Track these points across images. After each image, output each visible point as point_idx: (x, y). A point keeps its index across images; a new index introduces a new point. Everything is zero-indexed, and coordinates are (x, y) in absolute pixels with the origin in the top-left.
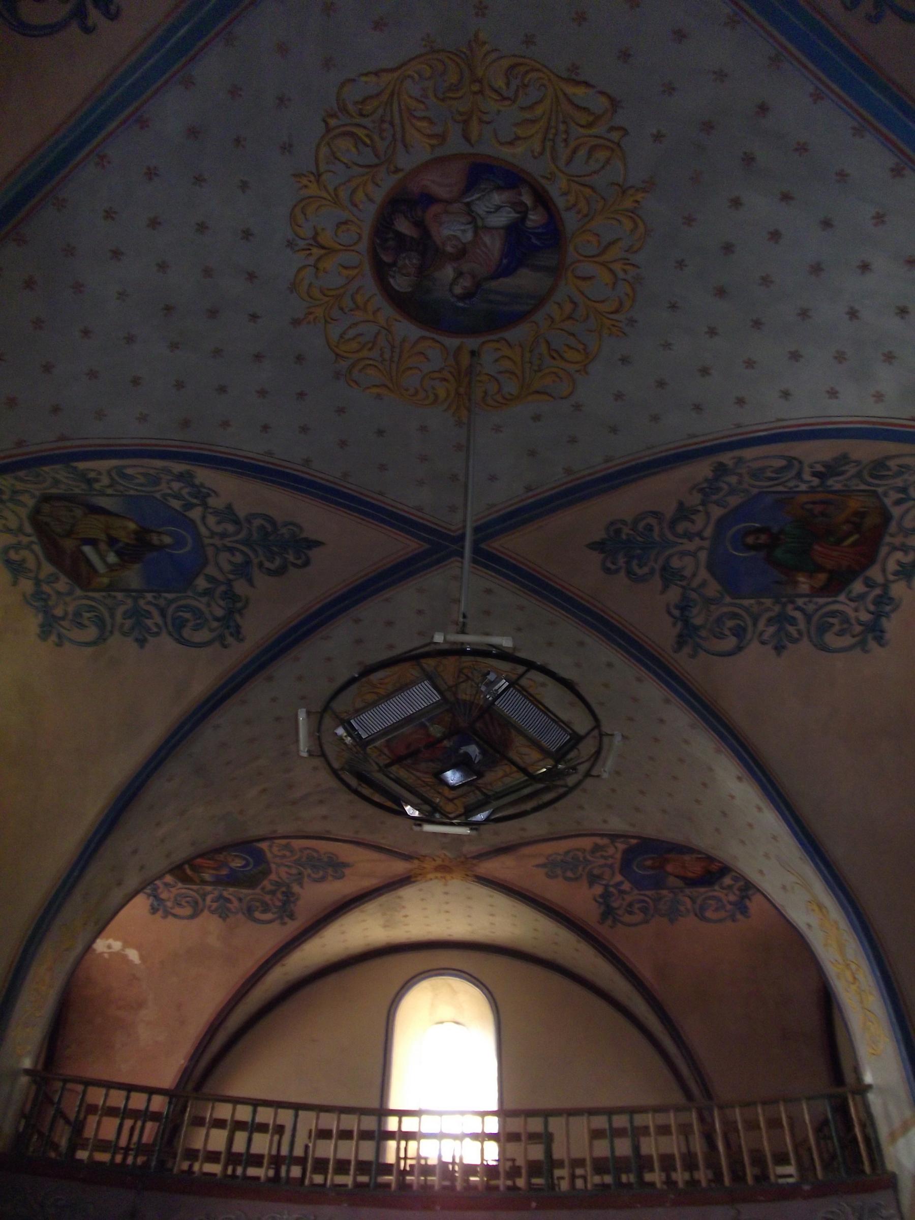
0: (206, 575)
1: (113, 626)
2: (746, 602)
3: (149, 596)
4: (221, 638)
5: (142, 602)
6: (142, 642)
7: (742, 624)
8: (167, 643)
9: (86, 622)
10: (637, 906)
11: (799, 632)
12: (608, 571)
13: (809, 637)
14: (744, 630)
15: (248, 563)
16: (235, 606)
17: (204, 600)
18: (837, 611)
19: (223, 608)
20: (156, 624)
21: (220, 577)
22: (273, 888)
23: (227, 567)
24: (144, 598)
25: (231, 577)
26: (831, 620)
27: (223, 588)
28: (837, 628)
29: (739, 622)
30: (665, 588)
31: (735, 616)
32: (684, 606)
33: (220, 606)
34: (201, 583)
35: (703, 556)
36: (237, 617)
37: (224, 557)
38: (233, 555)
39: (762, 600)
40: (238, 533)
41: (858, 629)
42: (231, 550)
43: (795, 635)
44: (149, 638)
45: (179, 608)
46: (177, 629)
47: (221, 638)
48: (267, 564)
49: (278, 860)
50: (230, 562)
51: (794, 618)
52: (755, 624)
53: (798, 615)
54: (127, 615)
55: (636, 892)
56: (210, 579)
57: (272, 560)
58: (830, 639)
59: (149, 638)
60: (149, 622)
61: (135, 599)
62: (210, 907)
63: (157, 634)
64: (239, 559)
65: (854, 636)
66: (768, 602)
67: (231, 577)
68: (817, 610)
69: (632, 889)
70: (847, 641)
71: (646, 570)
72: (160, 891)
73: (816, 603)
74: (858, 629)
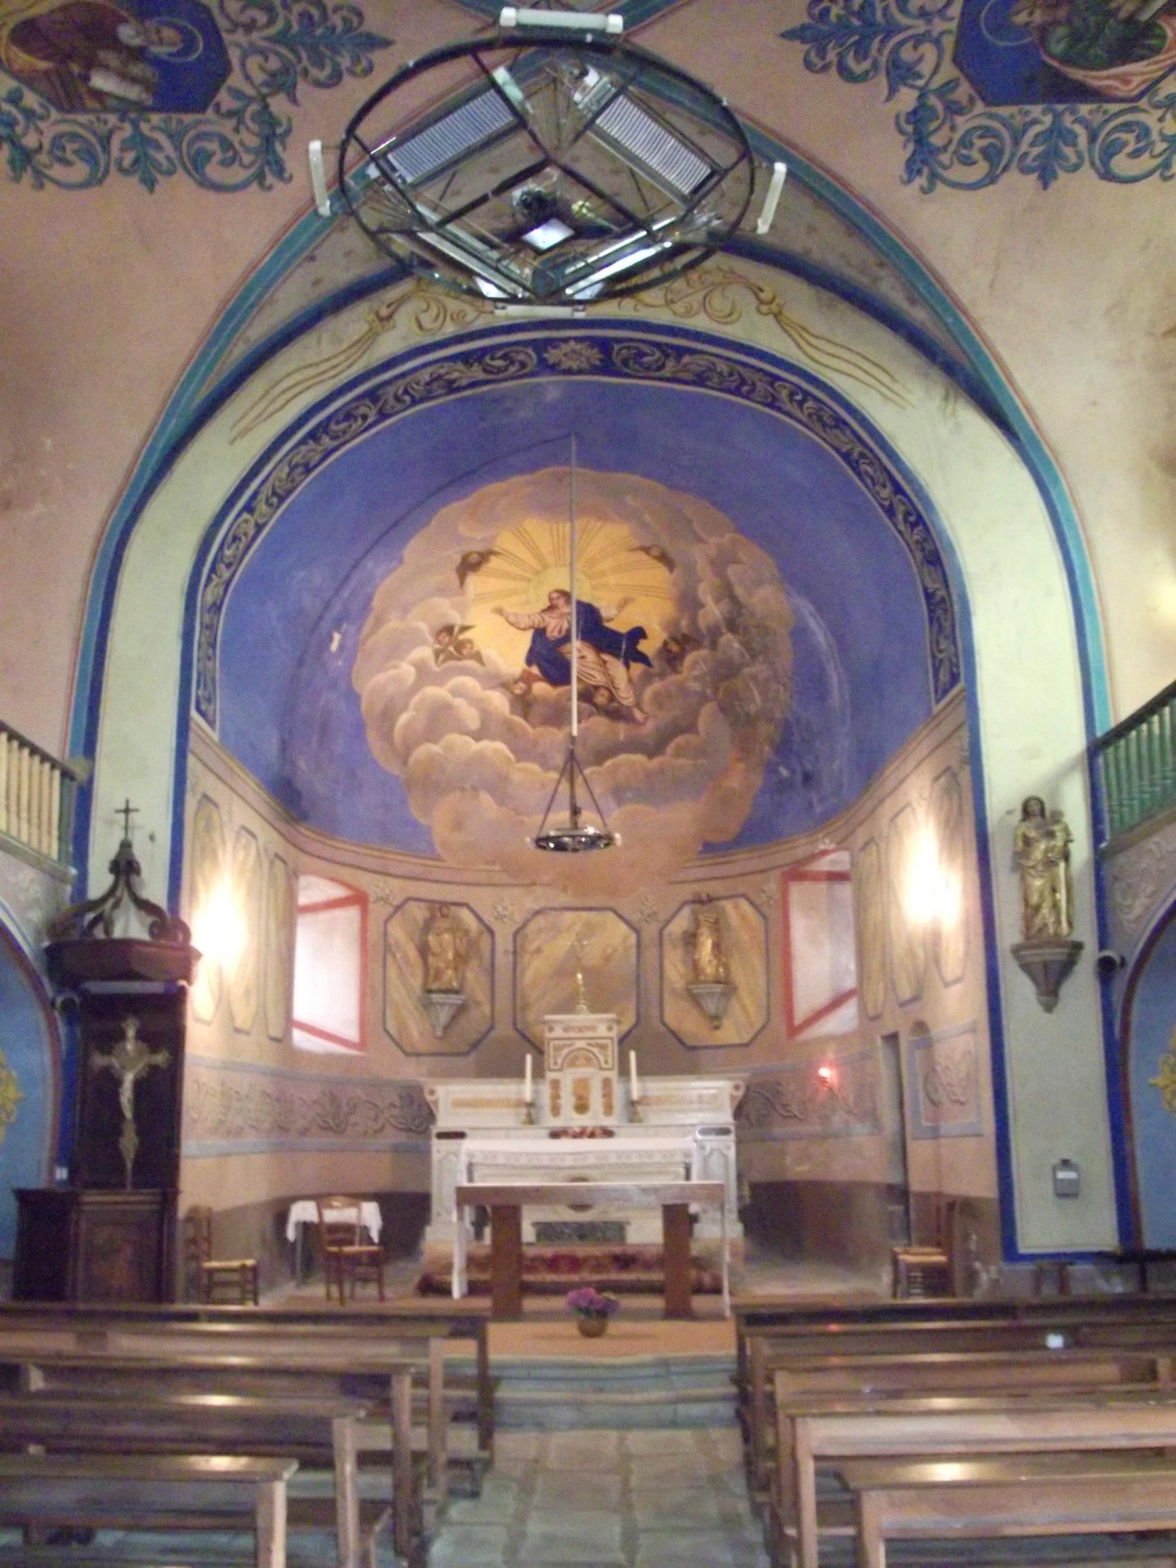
0: (230, 89)
1: (108, 165)
2: (1005, 111)
3: (156, 118)
4: (260, 177)
5: (145, 127)
6: (150, 184)
7: (998, 143)
8: (182, 183)
9: (70, 156)
10: (980, 143)
11: (1079, 155)
12: (808, 65)
13: (1093, 164)
14: (1000, 153)
15: (286, 69)
16: (272, 134)
17: (233, 122)
18: (1138, 123)
19: (257, 135)
20: (168, 158)
21: (250, 91)
22: (237, 105)
23: (259, 77)
24: (148, 121)
25: (264, 90)
26: (1124, 136)
27: (254, 107)
28: (1130, 148)
29: (991, 140)
30: (892, 90)
31: (987, 132)
32: (918, 117)
33: (253, 132)
34: (224, 98)
35: (949, 42)
36: (278, 147)
37: (253, 63)
38: (266, 59)
39: (1027, 107)
40: (271, 22)
41: (1160, 147)
42: (263, 53)
43: (1074, 159)
44: (159, 177)
45: (198, 137)
46: (196, 164)
47: (260, 177)
48: (314, 72)
49: (240, 37)
50: (262, 68)
51: (1071, 132)
52: (1016, 142)
53: (1079, 130)
54: (126, 146)
55: (980, 107)
56: (237, 94)
57: (322, 67)
58: (1121, 164)
59: (159, 177)
60: (160, 157)
61: (135, 124)
62: (119, 163)
63: (170, 173)
64: (274, 64)
65: (1153, 157)
66: (1036, 110)
67: (264, 90)
68: (1107, 121)
69: (972, 100)
70: (1146, 162)
71: (866, 65)
72: (19, 130)
73: (1105, 112)
74: (1160, 147)
